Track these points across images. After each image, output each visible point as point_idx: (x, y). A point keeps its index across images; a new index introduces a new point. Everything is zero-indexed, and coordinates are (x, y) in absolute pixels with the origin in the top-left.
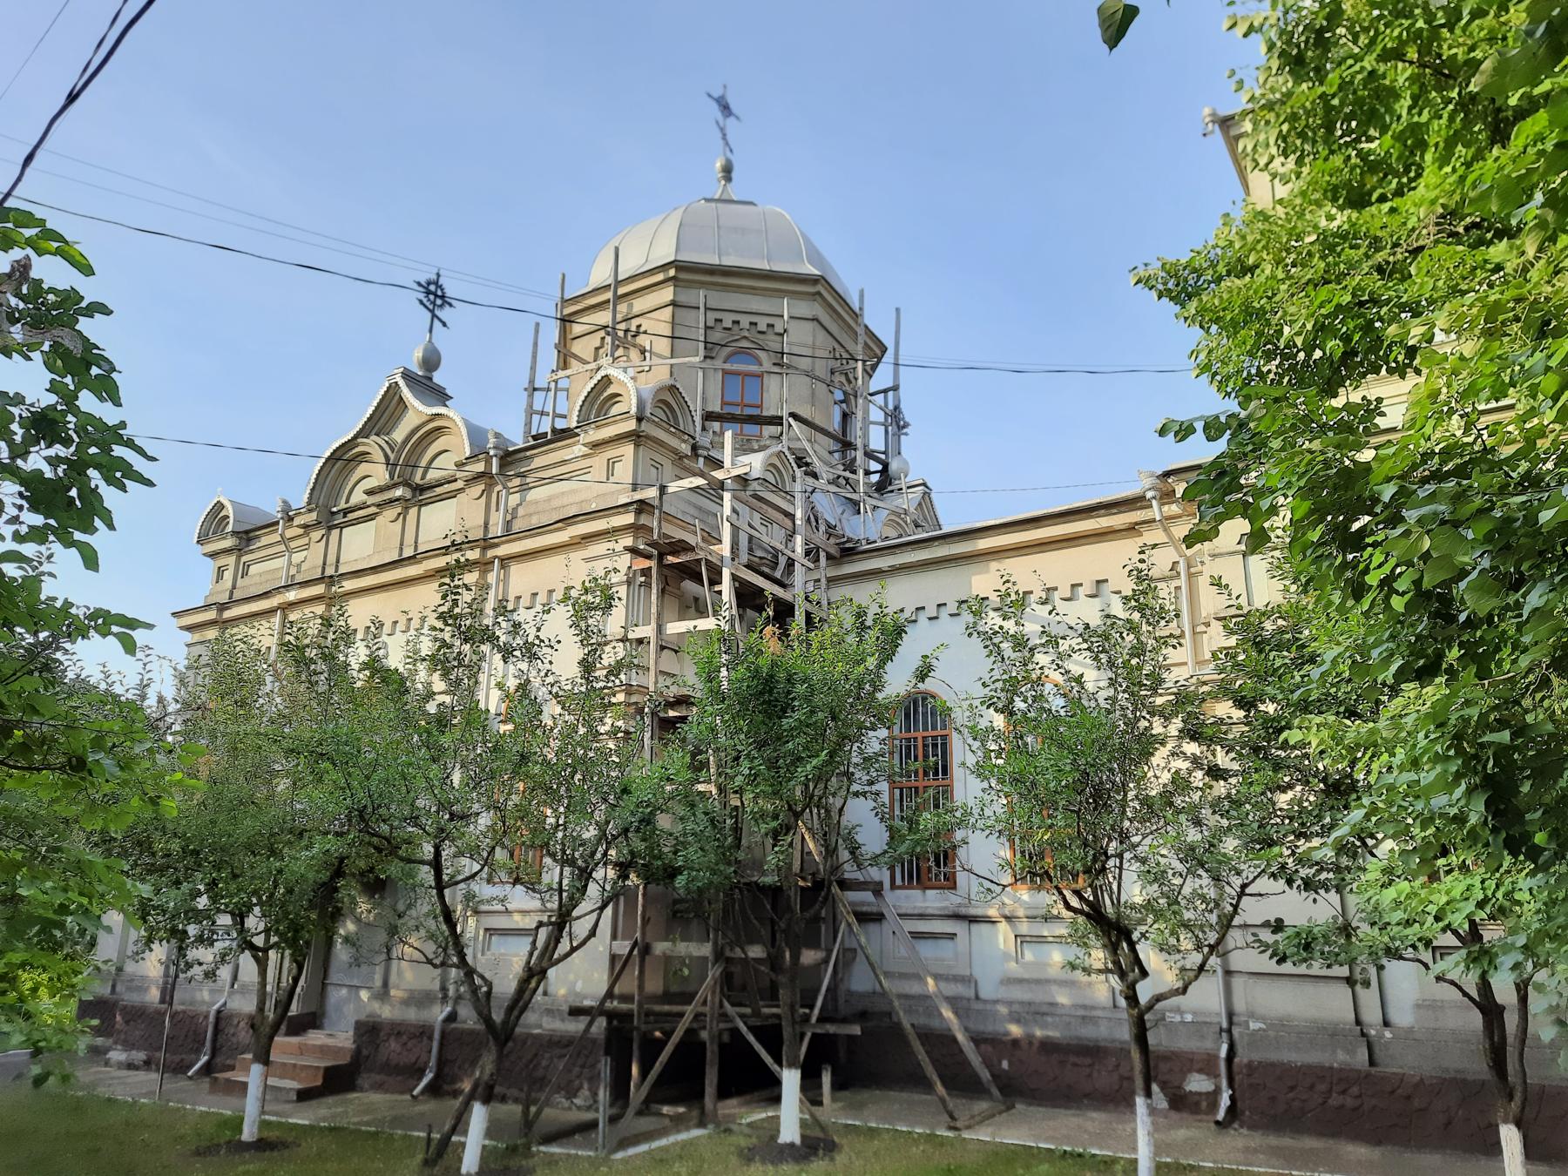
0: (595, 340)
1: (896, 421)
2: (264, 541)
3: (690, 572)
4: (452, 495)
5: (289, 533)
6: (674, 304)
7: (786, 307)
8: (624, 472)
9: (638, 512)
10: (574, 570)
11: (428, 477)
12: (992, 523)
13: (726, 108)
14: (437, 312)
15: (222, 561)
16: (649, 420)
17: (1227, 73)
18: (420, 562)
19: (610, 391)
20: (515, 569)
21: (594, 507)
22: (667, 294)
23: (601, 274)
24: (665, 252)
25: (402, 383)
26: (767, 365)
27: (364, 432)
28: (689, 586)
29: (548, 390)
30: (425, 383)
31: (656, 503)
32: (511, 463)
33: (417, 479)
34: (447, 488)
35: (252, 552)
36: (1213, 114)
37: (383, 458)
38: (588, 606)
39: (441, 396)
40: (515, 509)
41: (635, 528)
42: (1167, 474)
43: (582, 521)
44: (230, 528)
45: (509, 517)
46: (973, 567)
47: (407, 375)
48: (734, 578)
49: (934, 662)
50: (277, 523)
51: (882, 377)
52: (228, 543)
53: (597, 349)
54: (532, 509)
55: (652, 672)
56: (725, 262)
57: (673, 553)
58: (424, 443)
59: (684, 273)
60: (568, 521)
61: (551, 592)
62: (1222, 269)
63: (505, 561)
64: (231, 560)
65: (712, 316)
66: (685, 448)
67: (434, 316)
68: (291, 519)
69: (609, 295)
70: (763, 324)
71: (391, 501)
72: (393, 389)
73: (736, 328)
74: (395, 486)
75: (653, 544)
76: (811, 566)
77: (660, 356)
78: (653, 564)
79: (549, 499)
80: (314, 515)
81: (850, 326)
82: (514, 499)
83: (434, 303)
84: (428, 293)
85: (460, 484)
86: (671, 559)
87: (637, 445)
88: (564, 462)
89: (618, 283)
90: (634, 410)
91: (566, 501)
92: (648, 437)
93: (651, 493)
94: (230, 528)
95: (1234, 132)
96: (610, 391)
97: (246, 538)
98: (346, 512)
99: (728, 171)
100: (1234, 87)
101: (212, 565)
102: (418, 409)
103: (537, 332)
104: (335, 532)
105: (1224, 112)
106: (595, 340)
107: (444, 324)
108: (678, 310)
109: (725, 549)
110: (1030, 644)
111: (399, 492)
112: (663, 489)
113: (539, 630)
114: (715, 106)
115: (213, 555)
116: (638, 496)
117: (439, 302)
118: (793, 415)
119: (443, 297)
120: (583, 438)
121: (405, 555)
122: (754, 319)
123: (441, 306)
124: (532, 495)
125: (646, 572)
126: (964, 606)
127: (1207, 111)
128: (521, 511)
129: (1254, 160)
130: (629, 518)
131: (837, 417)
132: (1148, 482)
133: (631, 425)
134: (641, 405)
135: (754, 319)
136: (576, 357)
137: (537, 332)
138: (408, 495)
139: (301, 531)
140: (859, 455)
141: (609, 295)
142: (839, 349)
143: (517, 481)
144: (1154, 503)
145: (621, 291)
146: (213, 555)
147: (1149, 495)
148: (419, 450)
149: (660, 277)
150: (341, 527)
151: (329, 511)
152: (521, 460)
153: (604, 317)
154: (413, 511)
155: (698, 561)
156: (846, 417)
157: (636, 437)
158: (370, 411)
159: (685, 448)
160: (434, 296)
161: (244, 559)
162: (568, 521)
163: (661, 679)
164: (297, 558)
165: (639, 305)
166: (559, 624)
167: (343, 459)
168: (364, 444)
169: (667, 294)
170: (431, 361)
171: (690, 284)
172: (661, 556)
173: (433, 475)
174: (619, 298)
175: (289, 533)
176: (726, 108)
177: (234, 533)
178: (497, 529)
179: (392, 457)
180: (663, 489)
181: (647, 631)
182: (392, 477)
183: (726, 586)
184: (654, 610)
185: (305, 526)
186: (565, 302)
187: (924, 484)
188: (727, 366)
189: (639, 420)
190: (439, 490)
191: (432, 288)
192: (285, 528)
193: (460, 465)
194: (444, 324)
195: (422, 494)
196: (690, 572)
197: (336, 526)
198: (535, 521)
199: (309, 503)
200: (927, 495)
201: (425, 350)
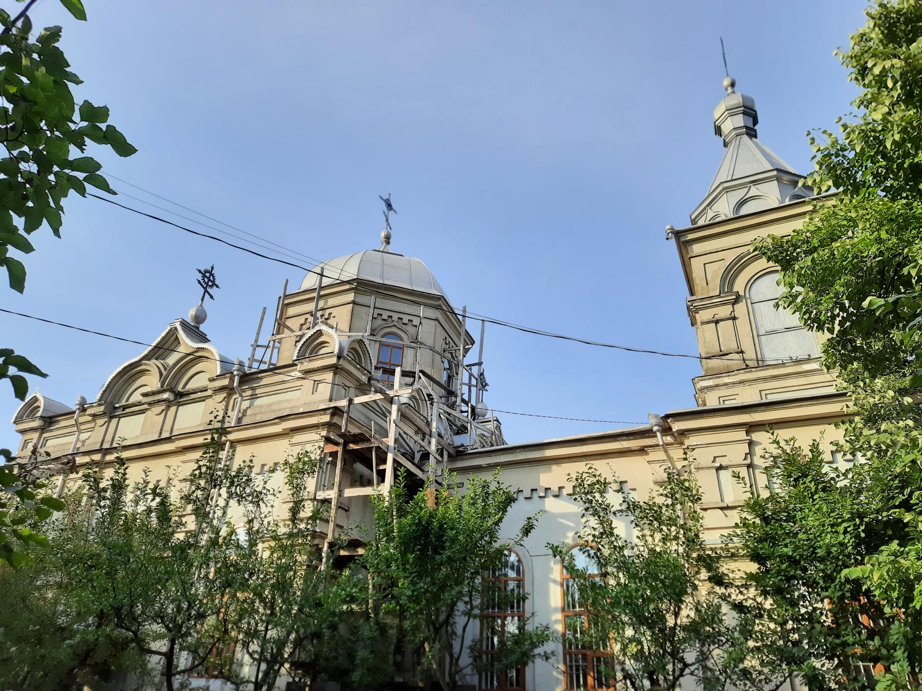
0: (301, 320)
1: (482, 384)
2: (62, 424)
3: (363, 457)
4: (203, 399)
5: (81, 420)
6: (354, 302)
7: (422, 311)
8: (325, 390)
9: (333, 415)
10: (282, 451)
11: (188, 387)
12: (554, 440)
13: (389, 206)
14: (208, 289)
15: (28, 436)
16: (345, 359)
17: (806, 133)
18: (173, 441)
19: (321, 340)
20: (240, 449)
21: (301, 410)
22: (350, 297)
23: (311, 281)
24: (351, 272)
25: (179, 328)
26: (406, 342)
27: (147, 357)
28: (360, 467)
29: (268, 347)
30: (194, 330)
31: (346, 409)
32: (247, 381)
33: (180, 388)
34: (200, 395)
35: (51, 431)
36: (672, 229)
37: (169, 367)
38: (298, 471)
39: (203, 338)
40: (245, 411)
41: (329, 425)
42: (668, 416)
43: (293, 419)
44: (39, 414)
45: (240, 415)
46: (540, 468)
47: (184, 324)
48: (395, 461)
49: (535, 522)
50: (74, 412)
51: (472, 357)
52: (37, 423)
53: (302, 325)
54: (257, 411)
55: (331, 525)
56: (386, 282)
57: (355, 443)
58: (188, 366)
59: (361, 286)
60: (282, 418)
61: (263, 466)
62: (815, 242)
63: (233, 444)
64: (36, 435)
65: (377, 311)
66: (364, 379)
67: (206, 291)
68: (84, 410)
69: (315, 294)
70: (406, 319)
71: (159, 401)
72: (173, 331)
73: (390, 320)
74: (163, 391)
75: (342, 436)
76: (440, 459)
77: (343, 331)
78: (340, 449)
79: (270, 405)
80: (102, 408)
81: (455, 327)
82: (246, 404)
83: (207, 284)
84: (204, 276)
85: (209, 392)
86: (352, 446)
87: (335, 374)
88: (283, 382)
89: (322, 288)
90: (336, 351)
91: (281, 406)
92: (343, 369)
93: (343, 403)
94: (39, 414)
95: (682, 239)
96: (321, 340)
97: (49, 421)
98: (124, 407)
99: (388, 239)
100: (809, 142)
101: (20, 438)
102: (187, 344)
103: (264, 313)
104: (115, 421)
105: (677, 228)
106: (301, 320)
107: (212, 297)
108: (356, 306)
109: (390, 441)
110: (613, 510)
111: (166, 396)
112: (351, 401)
113: (265, 483)
114: (384, 204)
115: (23, 432)
116: (333, 404)
117: (210, 283)
118: (421, 371)
119: (213, 282)
120: (299, 367)
121: (163, 436)
122: (401, 316)
123: (211, 286)
124: (258, 402)
125: (334, 454)
126: (534, 493)
127: (668, 227)
128: (249, 412)
129: (819, 188)
130: (326, 418)
131: (445, 378)
132: (653, 421)
133: (334, 360)
134: (341, 349)
135: (401, 316)
136: (288, 328)
137: (264, 313)
138: (172, 397)
139: (90, 418)
140: (459, 399)
141: (315, 294)
142: (449, 339)
143: (249, 393)
144: (658, 434)
145: (322, 293)
146: (23, 432)
147: (655, 429)
148: (184, 370)
149: (347, 287)
150: (119, 417)
151: (113, 405)
152: (254, 379)
153: (311, 307)
154: (173, 409)
155: (370, 449)
156: (450, 377)
157: (335, 368)
158: (163, 335)
159: (364, 379)
160: (208, 280)
161: (45, 435)
162: (282, 418)
163: (337, 530)
164: (83, 436)
165: (332, 301)
166: (279, 480)
167: (131, 373)
168: (146, 364)
169: (350, 297)
170: (200, 318)
171: (364, 293)
172: (345, 444)
173: (190, 386)
174: (320, 297)
175: (81, 420)
176: (389, 206)
177: (42, 417)
178: (232, 422)
179: (164, 373)
180: (351, 401)
181: (332, 494)
182: (162, 386)
183: (389, 467)
184: (337, 479)
185: (95, 416)
186: (286, 296)
187: (497, 420)
188: (384, 340)
189: (339, 357)
190: (193, 396)
191: (208, 275)
192: (79, 416)
193: (211, 380)
194: (212, 297)
195: (180, 397)
196: (363, 457)
197: (116, 416)
198: (258, 418)
199: (100, 400)
200: (498, 428)
201: (197, 311)
